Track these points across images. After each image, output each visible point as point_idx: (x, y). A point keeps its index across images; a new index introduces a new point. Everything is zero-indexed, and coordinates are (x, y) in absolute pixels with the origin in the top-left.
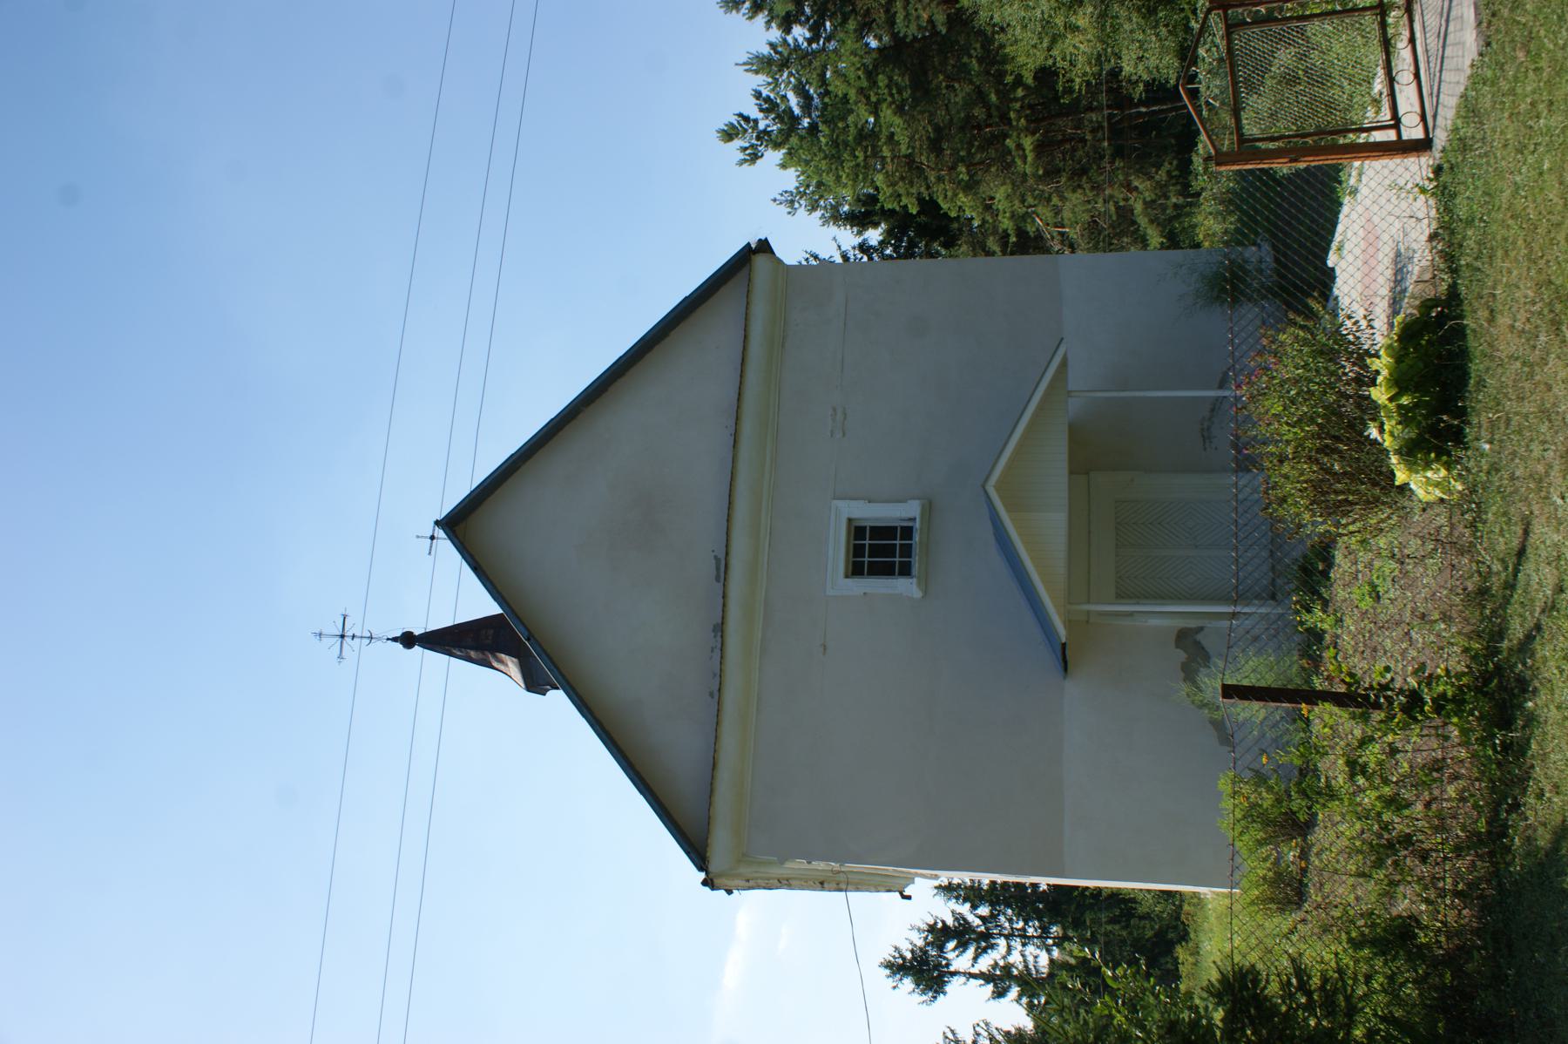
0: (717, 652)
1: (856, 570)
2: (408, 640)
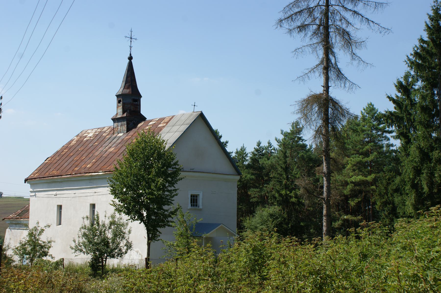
1: (191, 196)
2: (130, 58)
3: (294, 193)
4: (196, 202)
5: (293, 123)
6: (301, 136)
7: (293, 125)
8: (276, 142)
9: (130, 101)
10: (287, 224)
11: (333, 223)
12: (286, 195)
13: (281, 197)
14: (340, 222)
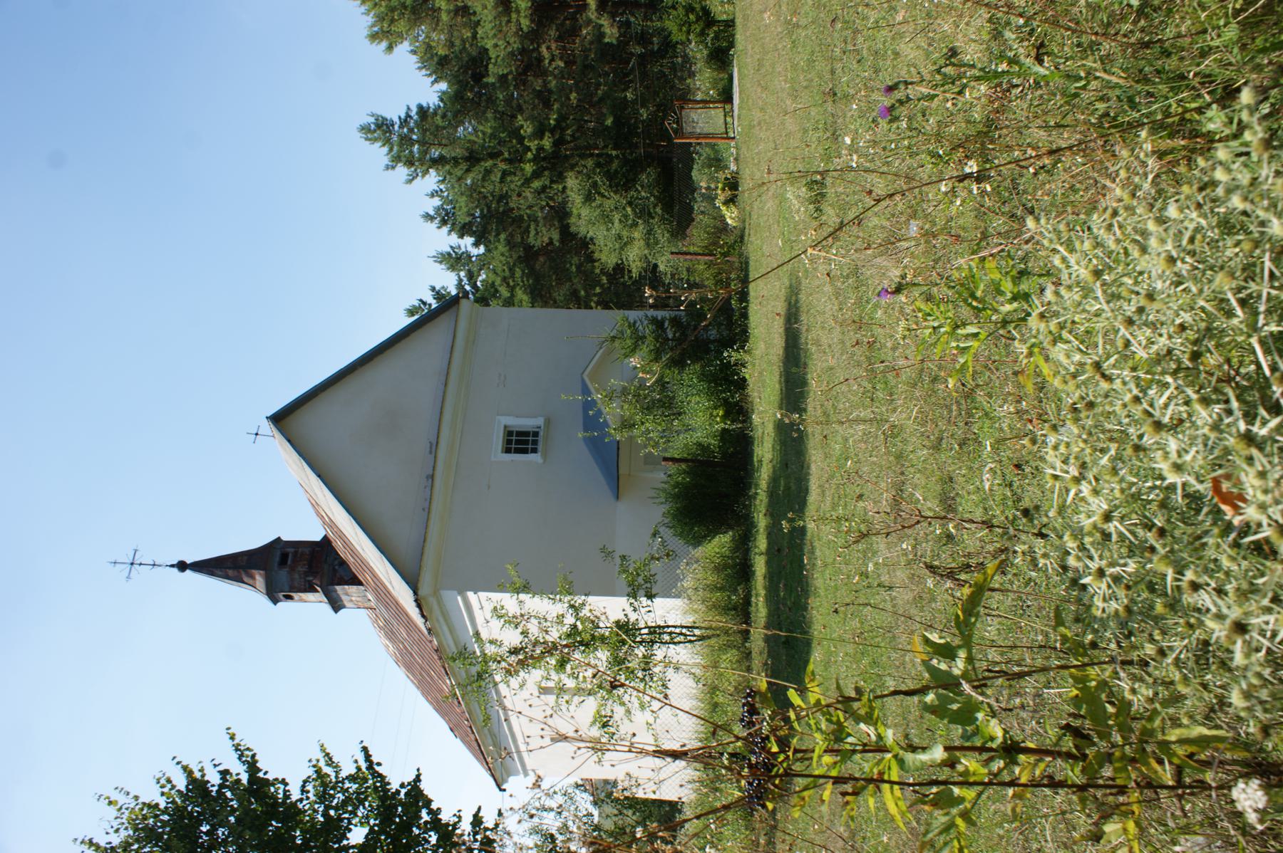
0: (428, 490)
1: (508, 451)
2: (182, 566)
3: (530, 140)
4: (526, 434)
5: (367, 139)
6: (396, 120)
7: (370, 140)
8: (415, 182)
9: (283, 575)
10: (610, 159)
11: (606, 40)
12: (535, 159)
13: (542, 172)
14: (605, 22)
